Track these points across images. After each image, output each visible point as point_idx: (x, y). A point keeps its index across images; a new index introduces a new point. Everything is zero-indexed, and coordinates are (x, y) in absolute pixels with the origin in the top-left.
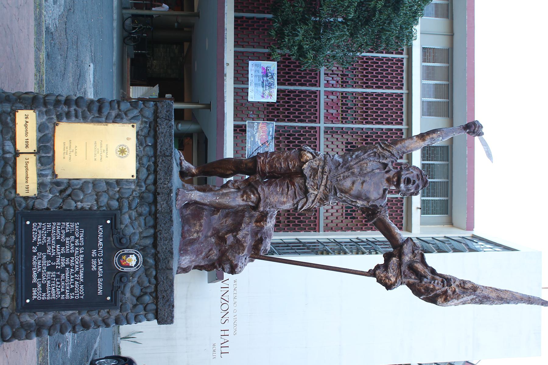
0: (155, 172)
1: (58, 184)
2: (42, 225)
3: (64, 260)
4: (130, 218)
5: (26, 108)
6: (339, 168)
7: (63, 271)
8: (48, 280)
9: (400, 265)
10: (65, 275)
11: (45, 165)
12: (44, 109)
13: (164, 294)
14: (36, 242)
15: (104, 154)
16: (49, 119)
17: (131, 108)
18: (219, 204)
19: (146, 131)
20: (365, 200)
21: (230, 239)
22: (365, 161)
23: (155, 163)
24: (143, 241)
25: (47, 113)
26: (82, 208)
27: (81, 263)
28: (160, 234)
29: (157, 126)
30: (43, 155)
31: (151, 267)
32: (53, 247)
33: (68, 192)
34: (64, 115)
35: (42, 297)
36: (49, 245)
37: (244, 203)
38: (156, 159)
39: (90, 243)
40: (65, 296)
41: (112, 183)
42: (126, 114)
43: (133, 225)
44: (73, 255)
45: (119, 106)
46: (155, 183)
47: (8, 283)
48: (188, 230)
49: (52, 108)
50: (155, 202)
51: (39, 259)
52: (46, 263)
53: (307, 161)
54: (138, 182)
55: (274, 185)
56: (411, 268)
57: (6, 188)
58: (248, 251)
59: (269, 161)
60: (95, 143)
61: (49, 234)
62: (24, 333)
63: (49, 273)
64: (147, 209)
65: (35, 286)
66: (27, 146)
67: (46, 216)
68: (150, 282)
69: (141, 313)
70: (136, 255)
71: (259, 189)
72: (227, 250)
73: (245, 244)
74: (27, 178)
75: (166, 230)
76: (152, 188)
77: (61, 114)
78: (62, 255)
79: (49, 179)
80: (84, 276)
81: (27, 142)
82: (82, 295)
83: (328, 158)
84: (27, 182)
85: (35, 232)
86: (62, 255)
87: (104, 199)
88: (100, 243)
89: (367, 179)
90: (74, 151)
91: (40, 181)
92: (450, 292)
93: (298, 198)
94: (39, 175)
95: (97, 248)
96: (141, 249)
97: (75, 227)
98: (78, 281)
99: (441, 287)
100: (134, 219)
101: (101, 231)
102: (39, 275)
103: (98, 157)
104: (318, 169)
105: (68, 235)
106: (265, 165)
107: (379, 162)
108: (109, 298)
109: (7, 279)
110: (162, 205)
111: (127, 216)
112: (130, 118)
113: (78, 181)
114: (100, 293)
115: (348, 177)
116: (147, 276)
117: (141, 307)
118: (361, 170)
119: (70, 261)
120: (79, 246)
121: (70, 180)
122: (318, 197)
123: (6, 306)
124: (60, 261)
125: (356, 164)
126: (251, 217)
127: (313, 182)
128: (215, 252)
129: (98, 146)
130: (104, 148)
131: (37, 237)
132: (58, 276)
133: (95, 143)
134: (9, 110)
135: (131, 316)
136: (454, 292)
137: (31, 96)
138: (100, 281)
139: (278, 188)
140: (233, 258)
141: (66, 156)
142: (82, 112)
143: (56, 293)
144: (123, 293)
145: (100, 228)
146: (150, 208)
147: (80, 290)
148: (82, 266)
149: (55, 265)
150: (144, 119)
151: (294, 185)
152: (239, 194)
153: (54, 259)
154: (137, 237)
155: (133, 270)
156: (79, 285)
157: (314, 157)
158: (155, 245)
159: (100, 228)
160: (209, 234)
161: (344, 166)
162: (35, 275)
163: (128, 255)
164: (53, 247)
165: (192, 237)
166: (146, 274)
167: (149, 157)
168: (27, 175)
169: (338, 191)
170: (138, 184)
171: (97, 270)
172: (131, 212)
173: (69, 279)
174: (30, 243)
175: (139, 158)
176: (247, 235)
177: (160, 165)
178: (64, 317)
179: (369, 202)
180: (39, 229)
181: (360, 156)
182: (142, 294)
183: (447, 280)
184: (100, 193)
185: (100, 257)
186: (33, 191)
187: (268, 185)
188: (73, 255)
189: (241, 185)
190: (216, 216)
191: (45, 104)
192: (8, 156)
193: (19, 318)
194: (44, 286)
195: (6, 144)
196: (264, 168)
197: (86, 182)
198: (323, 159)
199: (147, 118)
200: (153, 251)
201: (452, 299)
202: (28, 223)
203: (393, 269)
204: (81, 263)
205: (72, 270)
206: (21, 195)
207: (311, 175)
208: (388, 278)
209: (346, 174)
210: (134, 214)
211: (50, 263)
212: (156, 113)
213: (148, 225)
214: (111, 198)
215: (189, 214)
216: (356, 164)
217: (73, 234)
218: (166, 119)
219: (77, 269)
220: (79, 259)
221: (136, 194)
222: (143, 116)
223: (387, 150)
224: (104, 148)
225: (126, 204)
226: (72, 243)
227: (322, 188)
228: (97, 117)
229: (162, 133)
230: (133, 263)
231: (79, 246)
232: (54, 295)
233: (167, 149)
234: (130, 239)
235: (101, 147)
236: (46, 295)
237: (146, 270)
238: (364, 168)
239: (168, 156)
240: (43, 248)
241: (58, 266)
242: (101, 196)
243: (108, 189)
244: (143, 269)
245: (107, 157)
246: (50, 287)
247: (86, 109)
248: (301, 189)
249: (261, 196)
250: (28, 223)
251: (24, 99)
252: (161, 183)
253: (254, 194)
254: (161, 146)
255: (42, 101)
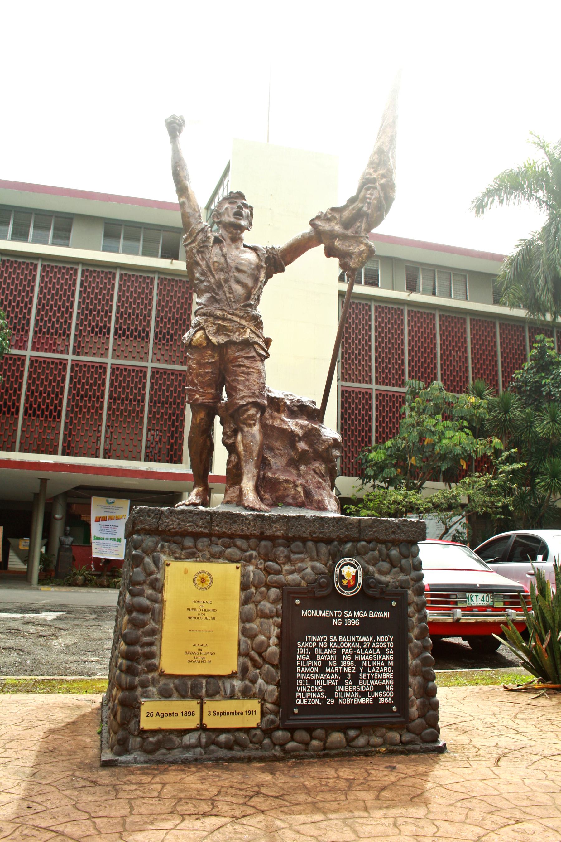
0: (232, 536)
1: (244, 670)
2: (300, 692)
3: (345, 663)
4: (292, 572)
5: (137, 716)
6: (218, 297)
7: (358, 663)
8: (369, 682)
9: (344, 237)
10: (364, 661)
11: (219, 687)
12: (140, 689)
13: (391, 530)
14: (321, 700)
15: (207, 606)
16: (153, 683)
17: (141, 566)
18: (258, 456)
19: (174, 547)
20: (259, 271)
21: (302, 445)
22: (211, 264)
23: (220, 536)
24: (322, 557)
25: (144, 685)
26: (278, 637)
27: (349, 639)
28: (315, 533)
29: (169, 530)
30: (204, 690)
31: (356, 547)
32: (328, 677)
33: (257, 657)
34: (149, 662)
35: (390, 691)
36: (325, 683)
37: (257, 423)
38: (215, 535)
39: (324, 627)
40: (390, 660)
41: (245, 596)
42: (151, 573)
43: (302, 570)
44: (339, 650)
45: (139, 583)
46: (246, 537)
47: (371, 735)
48: (294, 498)
49: (137, 679)
50: (272, 539)
51: (343, 695)
52: (349, 685)
53: (207, 338)
54: (245, 560)
55: (235, 384)
56: (346, 225)
57: (249, 742)
58: (316, 424)
59: (202, 388)
60: (190, 618)
61: (312, 682)
62: (431, 712)
63: (361, 682)
64: (281, 548)
65: (376, 699)
66: (192, 714)
67: (287, 685)
68: (373, 550)
69: (411, 562)
70: (342, 567)
71: (242, 402)
72: (316, 451)
73: (310, 427)
74: (235, 713)
75: (310, 526)
76: (253, 541)
77: (146, 667)
78: (339, 665)
79: (237, 683)
80: (365, 635)
81: (186, 713)
82: (389, 639)
83: (204, 311)
84: (242, 713)
85: (308, 701)
86: (339, 665)
87: (267, 606)
88: (325, 614)
89: (233, 265)
90: (200, 647)
91: (240, 694)
92: (383, 181)
93: (254, 354)
94: (232, 697)
95: (331, 618)
96: (333, 559)
97: (303, 648)
98: (371, 643)
99: (375, 191)
100: (293, 568)
101: (310, 613)
102: (364, 694)
103: (208, 614)
104: (219, 324)
105: (313, 657)
106: (207, 393)
107: (212, 247)
108: (394, 603)
109: (366, 737)
110: (278, 530)
111: (291, 577)
112: (155, 569)
113: (242, 643)
114: (386, 615)
115: (230, 288)
116: (366, 553)
117: (403, 561)
118: (222, 270)
119: (347, 654)
120: (328, 642)
121: (240, 654)
122: (253, 329)
123: (399, 737)
124: (346, 667)
125: (214, 276)
126: (272, 417)
127: (235, 333)
128: (317, 465)
129: (195, 614)
130: (197, 606)
131: (315, 698)
132: (365, 670)
133: (190, 618)
134: (138, 739)
135: (414, 574)
136: (383, 176)
137: (119, 709)
138: (373, 615)
139: (240, 378)
140: (326, 444)
141: (207, 660)
142: (145, 637)
143: (385, 672)
144: (387, 584)
145: (305, 613)
146: (280, 545)
147: (384, 641)
148: (353, 639)
149: (352, 673)
150: (158, 549)
151: (237, 358)
152: (246, 429)
153: (343, 676)
154: (318, 564)
155: (360, 572)
156: (376, 642)
157: (202, 328)
158: (328, 541)
159: (305, 613)
160: (294, 472)
161: (217, 291)
162: (364, 701)
163: (342, 577)
164: (328, 677)
165: (302, 494)
166: (365, 555)
167: (211, 543)
168: (232, 713)
169: (247, 302)
170: (249, 560)
171: (359, 618)
172: (284, 571)
173: (369, 655)
174: (323, 708)
175: (214, 557)
176: (297, 424)
177: (224, 530)
178: (414, 662)
179: (262, 267)
180: (304, 695)
181: (203, 270)
182: (388, 560)
183: (367, 184)
184: (259, 613)
185: (343, 614)
186: (254, 705)
187: (236, 392)
188: (339, 650)
189: (230, 428)
190: (272, 460)
191: (132, 688)
192: (204, 740)
193: (415, 720)
194: (379, 688)
195: (188, 743)
196: (210, 396)
197: (244, 632)
198: (205, 317)
199: (157, 544)
200: (336, 543)
201: (392, 179)
202: (296, 710)
203: (350, 246)
204: (349, 639)
205: (358, 652)
206: (259, 721)
207: (225, 335)
208: (361, 253)
209: (226, 289)
210: (287, 567)
211: (349, 680)
212: (149, 532)
213: (302, 549)
214: (265, 597)
215: (271, 496)
216: (214, 276)
217: (312, 650)
218: (160, 518)
219: (357, 645)
220: (344, 642)
221: (261, 563)
222: (155, 550)
223: (196, 236)
224: (197, 606)
225: (273, 578)
226: (323, 651)
227: (243, 322)
228: (153, 614)
229: (179, 524)
230: (352, 570)
231: (328, 642)
232: (388, 675)
233: (201, 519)
234: (320, 574)
235: (196, 610)
236: (388, 685)
237: (359, 554)
238: (220, 266)
239: (211, 518)
240: (329, 690)
241: (352, 669)
242: (262, 611)
243: (254, 602)
244: (358, 557)
245: (210, 602)
246: (378, 680)
247: (142, 630)
248: (242, 350)
249: (251, 400)
250: (296, 710)
251: (123, 718)
252: (248, 528)
253: (248, 410)
254: (197, 526)
255: (127, 693)
